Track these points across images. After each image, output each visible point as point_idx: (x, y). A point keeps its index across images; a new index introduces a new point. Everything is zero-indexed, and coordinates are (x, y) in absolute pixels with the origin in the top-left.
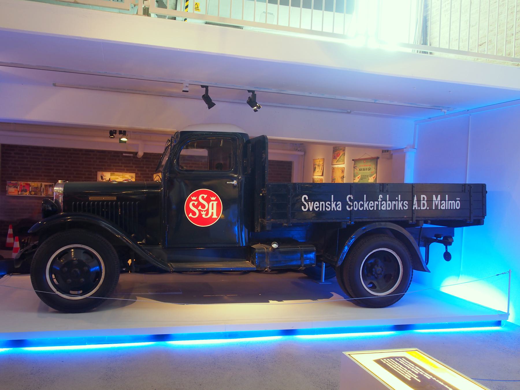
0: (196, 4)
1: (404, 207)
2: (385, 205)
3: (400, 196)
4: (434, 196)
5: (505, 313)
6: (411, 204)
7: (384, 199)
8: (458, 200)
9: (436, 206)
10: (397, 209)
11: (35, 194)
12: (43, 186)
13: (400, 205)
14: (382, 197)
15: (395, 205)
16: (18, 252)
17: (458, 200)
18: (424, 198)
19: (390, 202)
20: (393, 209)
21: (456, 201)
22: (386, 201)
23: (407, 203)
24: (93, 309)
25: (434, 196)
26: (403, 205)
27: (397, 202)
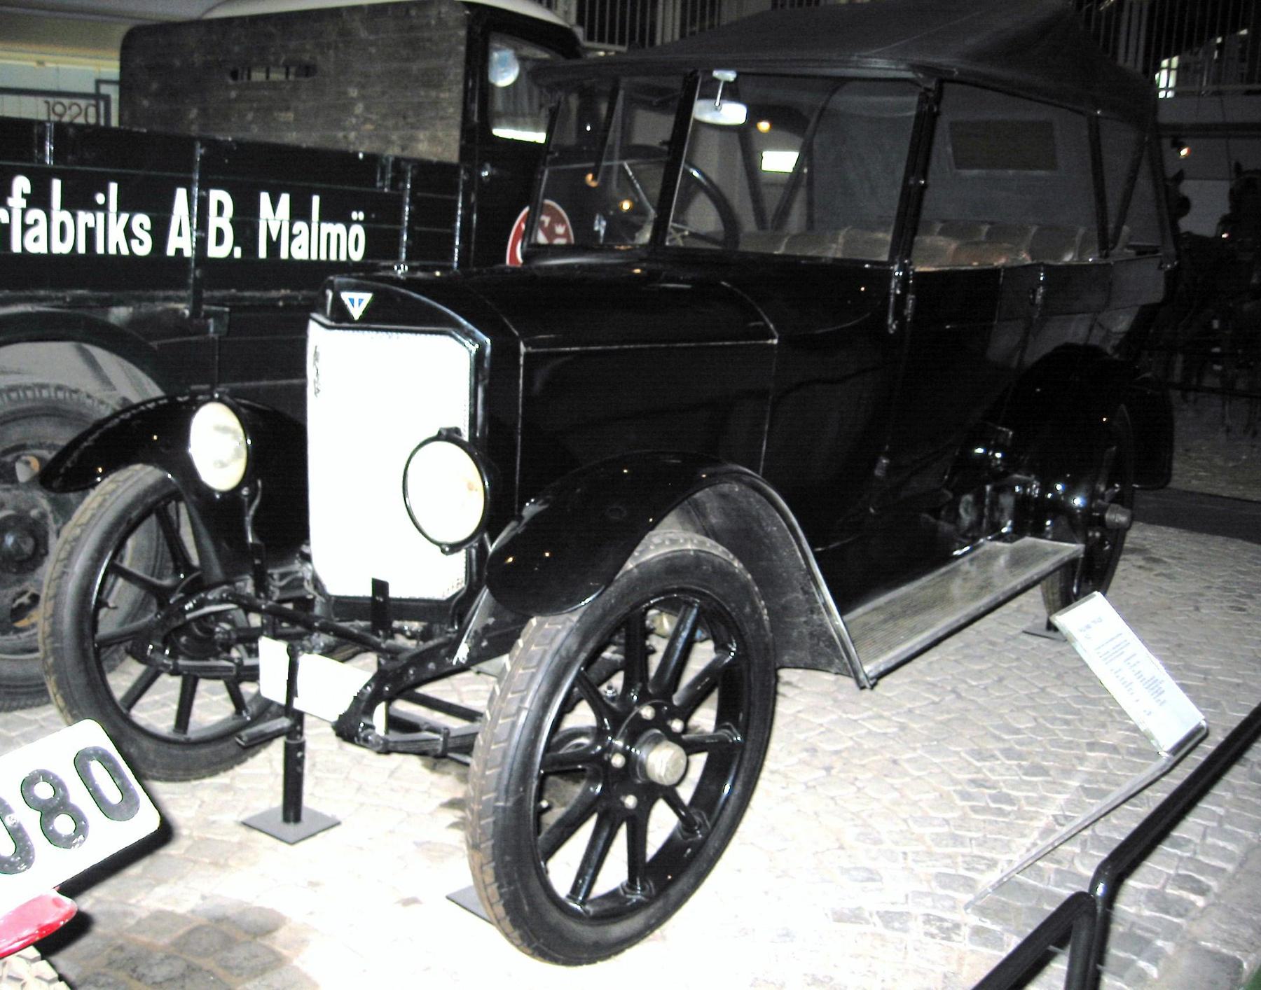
0: (752, 985)
1: (134, 243)
2: (41, 230)
3: (113, 187)
4: (265, 198)
5: (175, 518)
6: (160, 233)
7: (38, 199)
8: (358, 222)
9: (274, 246)
10: (100, 250)
11: (562, 222)
12: (676, 225)
13: (117, 234)
14: (28, 190)
15: (90, 233)
16: (372, 264)
17: (358, 222)
18: (220, 206)
19: (66, 216)
20: (82, 249)
21: (348, 223)
22: (47, 208)
23: (148, 226)
24: (718, 247)
25: (265, 198)
26: (129, 234)
27: (100, 215)
